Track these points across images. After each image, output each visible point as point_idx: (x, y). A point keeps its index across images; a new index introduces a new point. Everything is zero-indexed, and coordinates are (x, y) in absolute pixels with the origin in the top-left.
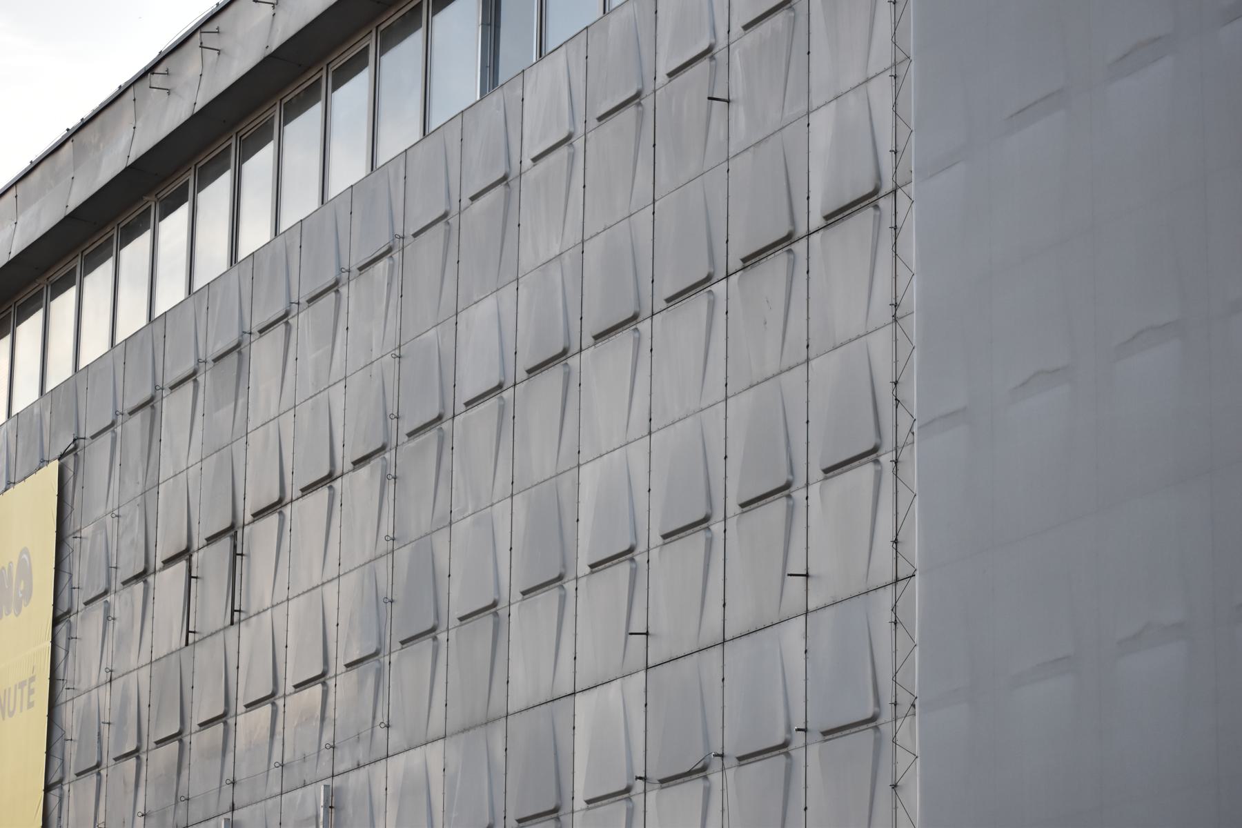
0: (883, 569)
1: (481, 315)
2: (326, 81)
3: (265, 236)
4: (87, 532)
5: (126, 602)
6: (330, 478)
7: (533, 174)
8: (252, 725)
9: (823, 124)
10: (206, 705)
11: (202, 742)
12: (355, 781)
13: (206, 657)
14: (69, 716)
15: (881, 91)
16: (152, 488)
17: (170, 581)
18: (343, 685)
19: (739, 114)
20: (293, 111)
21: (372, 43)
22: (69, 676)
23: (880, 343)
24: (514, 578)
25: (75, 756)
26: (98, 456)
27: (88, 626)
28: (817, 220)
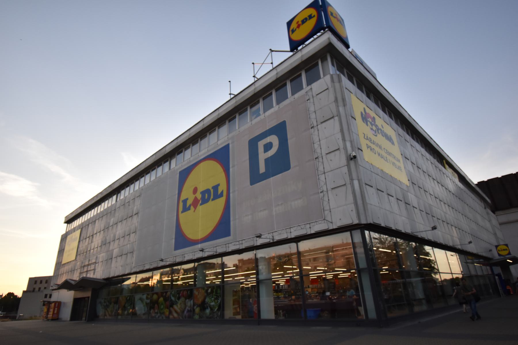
0: (135, 241)
1: (112, 219)
2: (151, 171)
3: (149, 181)
4: (82, 235)
5: (84, 241)
6: (132, 216)
7: (131, 201)
8: (92, 251)
9: (135, 207)
10: (89, 249)
11: (88, 252)
12: (98, 256)
13: (89, 245)
14: (79, 250)
15: (139, 205)
16: (87, 231)
17: (88, 239)
18: (99, 248)
19: (130, 206)
20: (132, 184)
21: (191, 145)
22: (353, 130)
23: (136, 224)
24: (112, 240)
25: (79, 253)
26: (84, 229)
27: (81, 242)
28: (134, 215)
